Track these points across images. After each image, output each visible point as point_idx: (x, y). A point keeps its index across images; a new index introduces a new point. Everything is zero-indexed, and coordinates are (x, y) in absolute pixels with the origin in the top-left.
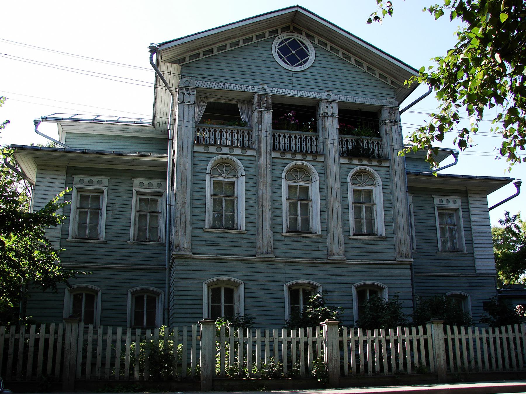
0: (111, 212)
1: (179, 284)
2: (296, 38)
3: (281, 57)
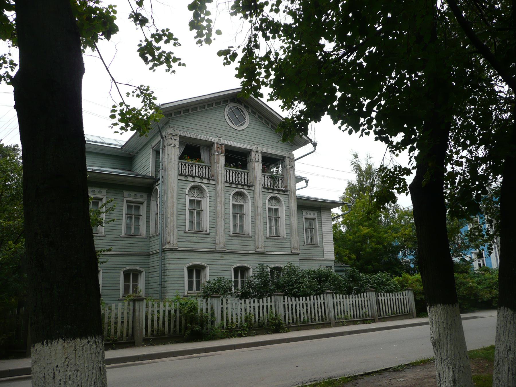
1: (169, 268)
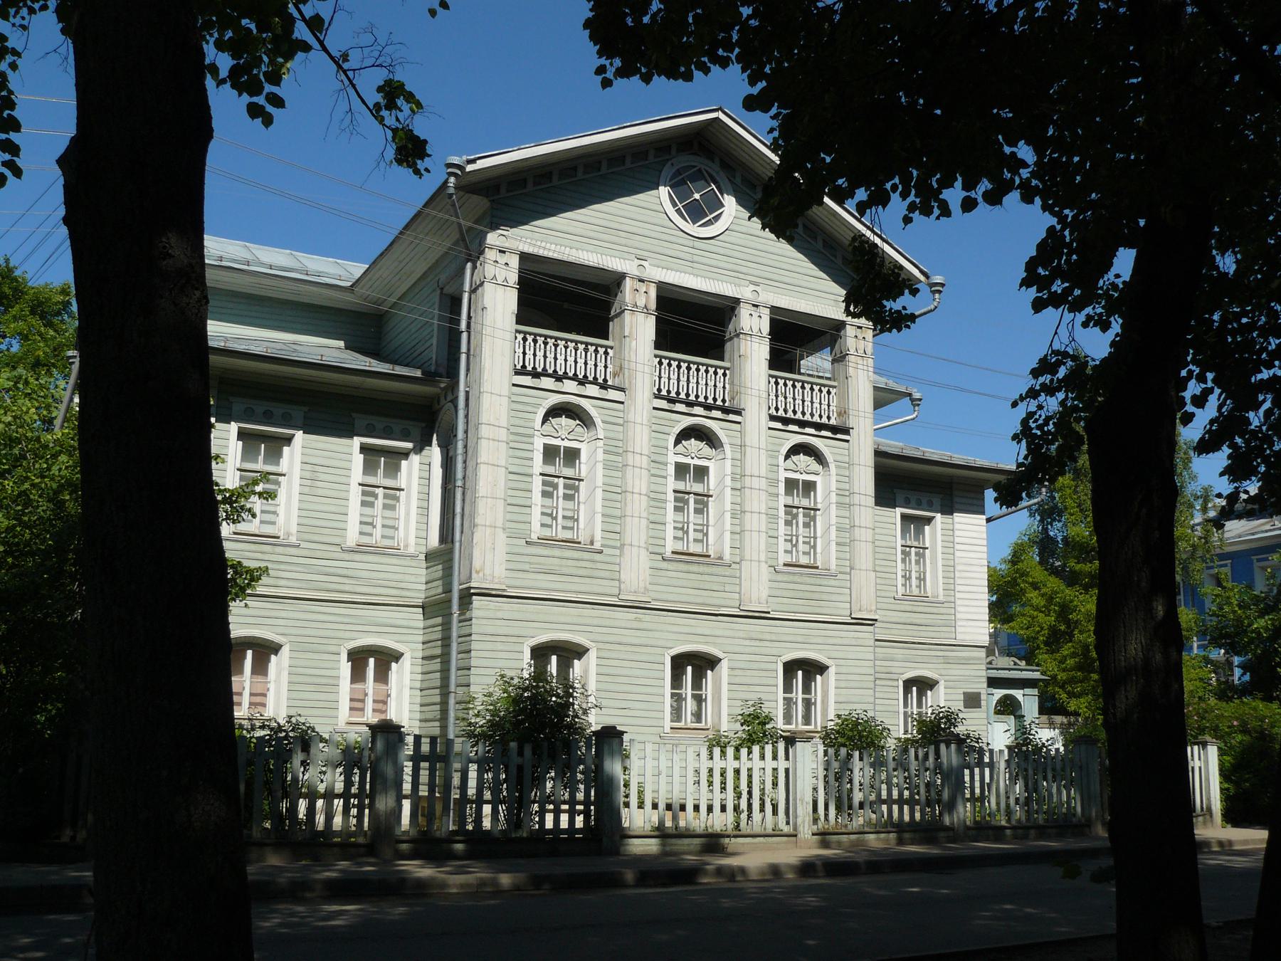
2: (703, 167)
3: (674, 205)
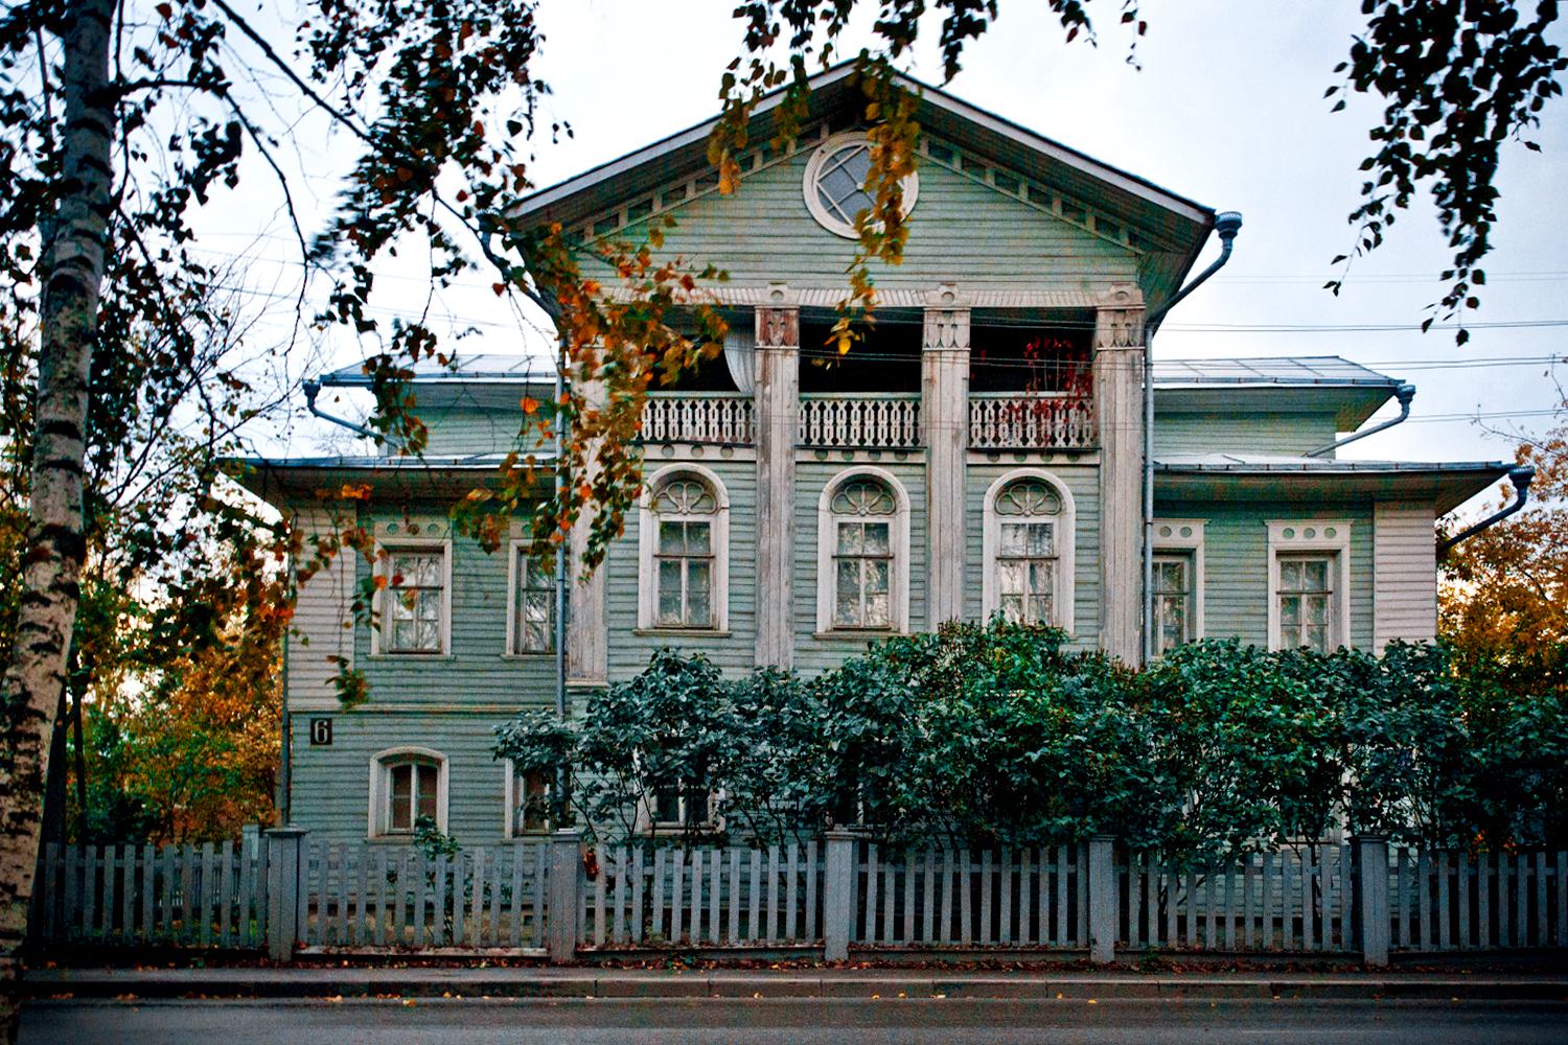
0: (462, 594)
